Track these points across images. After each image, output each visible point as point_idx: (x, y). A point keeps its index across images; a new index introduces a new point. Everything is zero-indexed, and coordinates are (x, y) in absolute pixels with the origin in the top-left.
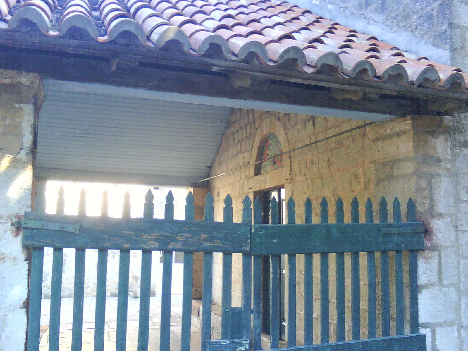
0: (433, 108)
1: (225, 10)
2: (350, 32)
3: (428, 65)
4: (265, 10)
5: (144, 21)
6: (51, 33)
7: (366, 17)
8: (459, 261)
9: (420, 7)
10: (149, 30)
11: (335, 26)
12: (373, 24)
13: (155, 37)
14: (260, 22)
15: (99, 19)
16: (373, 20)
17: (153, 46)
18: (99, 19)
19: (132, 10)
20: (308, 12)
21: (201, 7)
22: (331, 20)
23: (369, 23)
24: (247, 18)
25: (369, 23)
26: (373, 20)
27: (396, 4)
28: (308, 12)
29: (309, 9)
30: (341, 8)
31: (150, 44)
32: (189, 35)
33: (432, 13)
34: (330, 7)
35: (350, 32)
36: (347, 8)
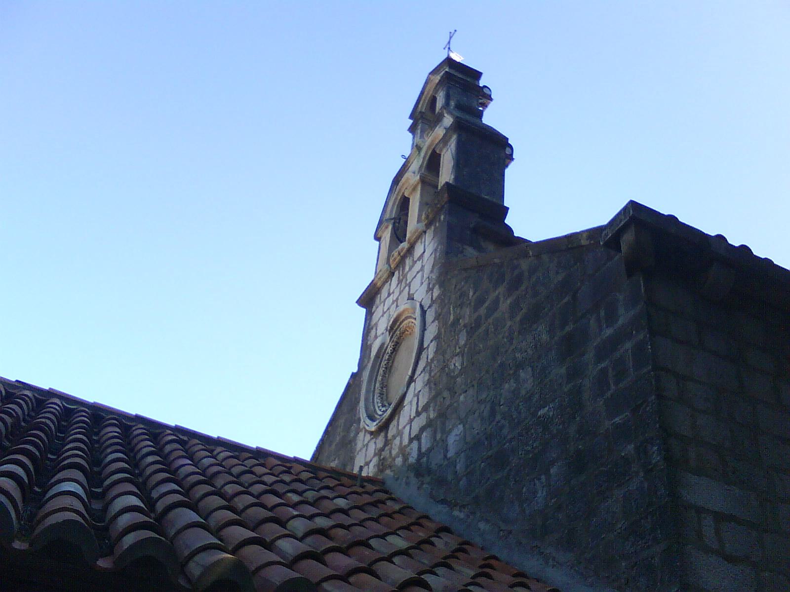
0: (423, 374)
1: (311, 518)
2: (515, 576)
3: (397, 286)
4: (376, 520)
5: (179, 532)
6: (17, 545)
7: (543, 553)
8: (387, 494)
9: (632, 550)
10: (186, 553)
11: (493, 562)
12: (553, 566)
13: (195, 569)
14: (370, 547)
15: (102, 520)
16: (554, 559)
17: (188, 586)
18: (102, 520)
19: (160, 506)
20: (446, 530)
21: (251, 467)
22: (482, 549)
23: (547, 563)
24: (349, 537)
25: (547, 563)
26: (554, 559)
27: (592, 539)
28: (446, 530)
29: (447, 525)
30: (501, 531)
31: (182, 582)
32: (253, 569)
33: (653, 561)
34: (482, 526)
35: (515, 576)
36: (510, 532)
